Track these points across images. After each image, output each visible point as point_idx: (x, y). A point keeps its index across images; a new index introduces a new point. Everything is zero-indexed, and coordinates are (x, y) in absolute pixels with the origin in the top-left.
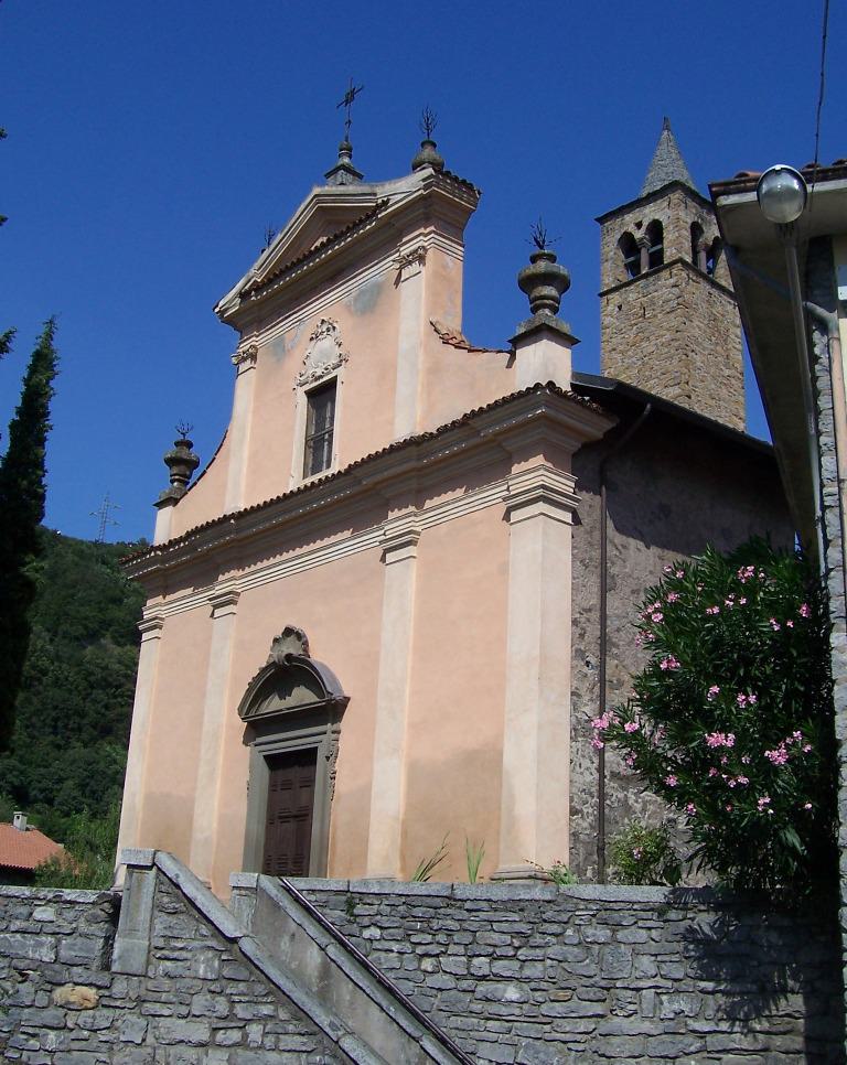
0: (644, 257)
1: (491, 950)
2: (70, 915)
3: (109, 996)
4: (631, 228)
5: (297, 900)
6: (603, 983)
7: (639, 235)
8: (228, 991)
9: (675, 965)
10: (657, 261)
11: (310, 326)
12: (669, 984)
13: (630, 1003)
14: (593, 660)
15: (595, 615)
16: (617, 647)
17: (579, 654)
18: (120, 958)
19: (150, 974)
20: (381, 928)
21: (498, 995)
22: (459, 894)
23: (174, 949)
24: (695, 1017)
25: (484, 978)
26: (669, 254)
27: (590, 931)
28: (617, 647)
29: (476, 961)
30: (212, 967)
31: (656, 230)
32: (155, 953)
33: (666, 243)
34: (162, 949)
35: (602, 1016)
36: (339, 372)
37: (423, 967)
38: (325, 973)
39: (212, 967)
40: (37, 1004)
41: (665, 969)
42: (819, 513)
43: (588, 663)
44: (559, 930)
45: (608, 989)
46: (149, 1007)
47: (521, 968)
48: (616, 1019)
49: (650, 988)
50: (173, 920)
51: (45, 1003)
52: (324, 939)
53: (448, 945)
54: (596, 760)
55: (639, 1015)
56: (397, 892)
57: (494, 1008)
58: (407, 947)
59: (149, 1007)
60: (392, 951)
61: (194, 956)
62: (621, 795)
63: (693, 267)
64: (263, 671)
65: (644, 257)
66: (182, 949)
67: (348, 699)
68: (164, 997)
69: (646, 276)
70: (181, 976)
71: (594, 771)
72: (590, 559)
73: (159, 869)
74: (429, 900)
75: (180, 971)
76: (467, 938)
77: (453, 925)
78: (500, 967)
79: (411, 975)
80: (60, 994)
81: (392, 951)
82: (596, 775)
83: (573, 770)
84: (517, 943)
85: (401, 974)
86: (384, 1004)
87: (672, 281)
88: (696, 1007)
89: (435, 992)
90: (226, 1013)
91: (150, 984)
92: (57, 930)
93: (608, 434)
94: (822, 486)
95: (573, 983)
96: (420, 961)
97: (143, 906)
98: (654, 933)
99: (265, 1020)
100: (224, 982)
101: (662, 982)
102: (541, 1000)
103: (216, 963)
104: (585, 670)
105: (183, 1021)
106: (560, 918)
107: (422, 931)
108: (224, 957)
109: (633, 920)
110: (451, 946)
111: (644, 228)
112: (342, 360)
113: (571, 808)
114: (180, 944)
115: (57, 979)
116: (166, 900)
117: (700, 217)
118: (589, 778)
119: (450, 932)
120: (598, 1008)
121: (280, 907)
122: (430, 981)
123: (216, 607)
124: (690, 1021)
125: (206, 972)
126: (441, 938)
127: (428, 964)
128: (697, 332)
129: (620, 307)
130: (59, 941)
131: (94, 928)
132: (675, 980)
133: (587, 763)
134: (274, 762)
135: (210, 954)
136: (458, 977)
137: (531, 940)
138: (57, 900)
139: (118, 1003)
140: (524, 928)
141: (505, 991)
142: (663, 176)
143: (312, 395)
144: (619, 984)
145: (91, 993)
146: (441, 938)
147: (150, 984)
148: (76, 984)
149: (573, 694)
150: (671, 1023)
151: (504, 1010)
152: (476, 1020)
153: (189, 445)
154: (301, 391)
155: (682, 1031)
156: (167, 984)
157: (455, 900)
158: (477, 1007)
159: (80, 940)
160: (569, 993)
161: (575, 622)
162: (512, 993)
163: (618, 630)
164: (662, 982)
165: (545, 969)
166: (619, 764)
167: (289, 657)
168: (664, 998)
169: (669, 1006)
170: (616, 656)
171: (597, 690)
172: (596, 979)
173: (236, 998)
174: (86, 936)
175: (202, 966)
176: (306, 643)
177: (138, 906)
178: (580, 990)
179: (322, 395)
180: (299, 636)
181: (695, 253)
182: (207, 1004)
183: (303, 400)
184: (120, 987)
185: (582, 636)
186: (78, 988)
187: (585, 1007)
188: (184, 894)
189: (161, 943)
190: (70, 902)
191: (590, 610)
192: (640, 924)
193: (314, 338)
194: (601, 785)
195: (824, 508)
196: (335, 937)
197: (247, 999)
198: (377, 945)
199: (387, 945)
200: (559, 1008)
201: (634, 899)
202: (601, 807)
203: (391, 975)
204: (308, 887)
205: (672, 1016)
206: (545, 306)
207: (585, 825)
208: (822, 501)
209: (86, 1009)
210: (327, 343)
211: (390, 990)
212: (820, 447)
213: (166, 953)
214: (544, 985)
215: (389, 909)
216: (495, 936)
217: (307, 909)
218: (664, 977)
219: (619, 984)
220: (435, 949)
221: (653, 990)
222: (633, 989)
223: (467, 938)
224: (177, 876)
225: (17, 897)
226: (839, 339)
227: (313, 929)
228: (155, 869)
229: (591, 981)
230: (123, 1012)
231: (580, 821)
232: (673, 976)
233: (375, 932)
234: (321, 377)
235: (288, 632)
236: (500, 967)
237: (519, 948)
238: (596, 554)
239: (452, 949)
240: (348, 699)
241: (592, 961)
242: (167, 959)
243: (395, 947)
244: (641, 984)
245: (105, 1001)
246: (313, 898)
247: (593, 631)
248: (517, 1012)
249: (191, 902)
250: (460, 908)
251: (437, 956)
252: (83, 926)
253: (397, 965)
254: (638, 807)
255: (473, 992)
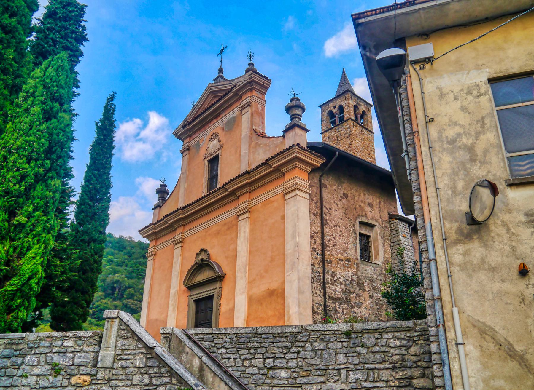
0: (337, 119)
1: (274, 355)
2: (79, 342)
3: (96, 379)
4: (332, 108)
5: (190, 338)
6: (323, 367)
7: (334, 111)
8: (150, 372)
9: (355, 358)
10: (342, 120)
11: (209, 135)
12: (352, 366)
13: (336, 376)
14: (320, 252)
15: (319, 235)
16: (329, 247)
17: (314, 250)
18: (101, 360)
19: (115, 367)
20: (226, 348)
21: (277, 375)
22: (259, 331)
23: (125, 355)
24: (366, 381)
25: (271, 368)
26: (346, 116)
27: (316, 344)
28: (329, 247)
29: (267, 361)
30: (142, 362)
31: (341, 108)
32: (117, 358)
33: (345, 113)
34: (120, 355)
35: (323, 382)
36: (220, 151)
37: (244, 365)
38: (201, 369)
39: (142, 362)
40: (63, 385)
41: (350, 360)
42: (405, 148)
43: (317, 254)
44: (303, 345)
45: (326, 370)
46: (114, 383)
47: (287, 362)
48: (330, 384)
49: (344, 368)
50: (126, 342)
51: (66, 384)
52: (201, 354)
53: (255, 354)
54: (322, 291)
55: (340, 381)
56: (233, 332)
57: (276, 381)
58: (237, 356)
59: (114, 383)
60: (231, 358)
61: (134, 357)
62: (333, 306)
63: (356, 121)
64: (193, 266)
65: (337, 119)
66: (129, 354)
67: (225, 274)
68: (120, 377)
69: (338, 125)
70: (128, 367)
71: (322, 296)
72: (317, 213)
73: (120, 319)
74: (246, 335)
75: (128, 365)
76: (264, 350)
77: (257, 345)
78: (278, 363)
79: (239, 369)
80: (74, 380)
81: (231, 358)
82: (323, 298)
83: (313, 296)
84: (285, 351)
85: (235, 368)
86: (227, 381)
87: (347, 126)
88: (365, 377)
89: (250, 376)
90: (148, 382)
91: (114, 372)
92: (74, 350)
93: (322, 165)
94: (405, 137)
95: (310, 368)
96: (243, 362)
97: (113, 336)
98: (345, 344)
99: (165, 384)
100: (147, 369)
101: (350, 366)
102: (296, 376)
103: (144, 360)
104: (317, 256)
105: (128, 388)
106: (303, 339)
107: (244, 349)
108: (148, 357)
109: (334, 339)
110: (257, 354)
111: (336, 108)
112: (221, 147)
113: (313, 310)
114: (128, 352)
115: (73, 372)
116: (123, 332)
117: (357, 103)
118: (320, 299)
119: (256, 348)
120: (322, 379)
121: (182, 341)
122: (248, 371)
123: (175, 245)
124: (363, 383)
125: (139, 364)
126: (252, 351)
127: (247, 363)
128: (357, 145)
129: (329, 138)
130: (75, 356)
131: (90, 348)
132: (355, 364)
133: (318, 293)
134: (197, 302)
135: (142, 356)
136: (259, 368)
137: (291, 350)
138: (75, 337)
139: (99, 382)
140: (288, 344)
141: (280, 373)
142: (343, 89)
143: (210, 161)
144: (330, 367)
145: (87, 378)
146: (252, 351)
147: (114, 372)
148: (81, 374)
149: (312, 265)
150: (355, 384)
151: (280, 382)
152: (268, 387)
153: (165, 186)
154: (206, 161)
155: (360, 387)
156: (121, 371)
157: (258, 334)
158: (268, 381)
159: (83, 354)
160: (309, 373)
161: (312, 237)
162: (283, 374)
163: (329, 241)
164: (350, 366)
165: (298, 363)
166: (332, 293)
167: (202, 260)
168: (350, 373)
169: (353, 377)
170: (329, 251)
171: (321, 263)
172: (320, 366)
173: (153, 375)
174: (87, 352)
175: (138, 362)
176: (209, 254)
177: (110, 336)
178: (314, 371)
179: (214, 161)
180: (206, 251)
181: (356, 116)
182: (139, 379)
183: (207, 163)
184: (100, 375)
185: (315, 242)
186: (82, 377)
187: (316, 379)
188: (131, 329)
189: (119, 352)
190: (80, 337)
191: (318, 233)
192: (338, 340)
193: (211, 140)
194: (325, 302)
195: (407, 145)
196: (207, 354)
197: (158, 375)
198: (224, 356)
199: (228, 356)
200: (305, 380)
201: (335, 329)
202: (325, 311)
203: (230, 369)
204: (195, 332)
205: (354, 381)
206: (296, 117)
207: (319, 317)
208: (406, 143)
209: (85, 386)
210: (215, 142)
211: (231, 376)
212: (403, 121)
213: (122, 356)
214: (298, 370)
215: (229, 340)
216: (275, 349)
217: (194, 342)
218: (350, 363)
219: (330, 367)
220: (250, 356)
221: (345, 370)
222: (336, 369)
223: (264, 350)
224: (128, 321)
225: (57, 337)
226: (410, 76)
227: (196, 350)
228: (117, 321)
229: (318, 367)
230: (101, 386)
231: (317, 316)
232: (354, 363)
233: (223, 350)
234: (213, 154)
235: (202, 250)
236: (278, 363)
237: (286, 353)
238: (319, 211)
239: (257, 356)
240: (225, 274)
241: (318, 358)
242: (122, 359)
243: (233, 356)
244: (340, 367)
245: (94, 382)
246: (197, 337)
247: (319, 240)
248: (286, 382)
249: (134, 333)
250: (260, 337)
251: (251, 359)
252: (85, 348)
253: (233, 364)
254: (340, 310)
255: (266, 374)
